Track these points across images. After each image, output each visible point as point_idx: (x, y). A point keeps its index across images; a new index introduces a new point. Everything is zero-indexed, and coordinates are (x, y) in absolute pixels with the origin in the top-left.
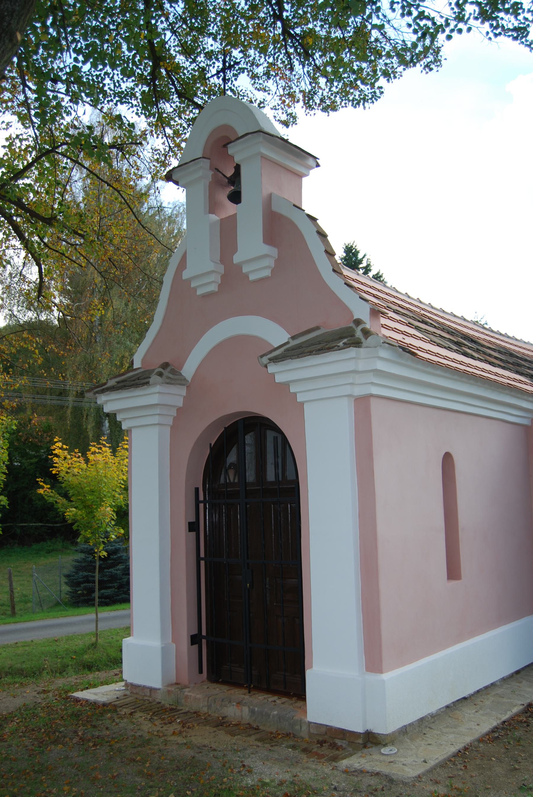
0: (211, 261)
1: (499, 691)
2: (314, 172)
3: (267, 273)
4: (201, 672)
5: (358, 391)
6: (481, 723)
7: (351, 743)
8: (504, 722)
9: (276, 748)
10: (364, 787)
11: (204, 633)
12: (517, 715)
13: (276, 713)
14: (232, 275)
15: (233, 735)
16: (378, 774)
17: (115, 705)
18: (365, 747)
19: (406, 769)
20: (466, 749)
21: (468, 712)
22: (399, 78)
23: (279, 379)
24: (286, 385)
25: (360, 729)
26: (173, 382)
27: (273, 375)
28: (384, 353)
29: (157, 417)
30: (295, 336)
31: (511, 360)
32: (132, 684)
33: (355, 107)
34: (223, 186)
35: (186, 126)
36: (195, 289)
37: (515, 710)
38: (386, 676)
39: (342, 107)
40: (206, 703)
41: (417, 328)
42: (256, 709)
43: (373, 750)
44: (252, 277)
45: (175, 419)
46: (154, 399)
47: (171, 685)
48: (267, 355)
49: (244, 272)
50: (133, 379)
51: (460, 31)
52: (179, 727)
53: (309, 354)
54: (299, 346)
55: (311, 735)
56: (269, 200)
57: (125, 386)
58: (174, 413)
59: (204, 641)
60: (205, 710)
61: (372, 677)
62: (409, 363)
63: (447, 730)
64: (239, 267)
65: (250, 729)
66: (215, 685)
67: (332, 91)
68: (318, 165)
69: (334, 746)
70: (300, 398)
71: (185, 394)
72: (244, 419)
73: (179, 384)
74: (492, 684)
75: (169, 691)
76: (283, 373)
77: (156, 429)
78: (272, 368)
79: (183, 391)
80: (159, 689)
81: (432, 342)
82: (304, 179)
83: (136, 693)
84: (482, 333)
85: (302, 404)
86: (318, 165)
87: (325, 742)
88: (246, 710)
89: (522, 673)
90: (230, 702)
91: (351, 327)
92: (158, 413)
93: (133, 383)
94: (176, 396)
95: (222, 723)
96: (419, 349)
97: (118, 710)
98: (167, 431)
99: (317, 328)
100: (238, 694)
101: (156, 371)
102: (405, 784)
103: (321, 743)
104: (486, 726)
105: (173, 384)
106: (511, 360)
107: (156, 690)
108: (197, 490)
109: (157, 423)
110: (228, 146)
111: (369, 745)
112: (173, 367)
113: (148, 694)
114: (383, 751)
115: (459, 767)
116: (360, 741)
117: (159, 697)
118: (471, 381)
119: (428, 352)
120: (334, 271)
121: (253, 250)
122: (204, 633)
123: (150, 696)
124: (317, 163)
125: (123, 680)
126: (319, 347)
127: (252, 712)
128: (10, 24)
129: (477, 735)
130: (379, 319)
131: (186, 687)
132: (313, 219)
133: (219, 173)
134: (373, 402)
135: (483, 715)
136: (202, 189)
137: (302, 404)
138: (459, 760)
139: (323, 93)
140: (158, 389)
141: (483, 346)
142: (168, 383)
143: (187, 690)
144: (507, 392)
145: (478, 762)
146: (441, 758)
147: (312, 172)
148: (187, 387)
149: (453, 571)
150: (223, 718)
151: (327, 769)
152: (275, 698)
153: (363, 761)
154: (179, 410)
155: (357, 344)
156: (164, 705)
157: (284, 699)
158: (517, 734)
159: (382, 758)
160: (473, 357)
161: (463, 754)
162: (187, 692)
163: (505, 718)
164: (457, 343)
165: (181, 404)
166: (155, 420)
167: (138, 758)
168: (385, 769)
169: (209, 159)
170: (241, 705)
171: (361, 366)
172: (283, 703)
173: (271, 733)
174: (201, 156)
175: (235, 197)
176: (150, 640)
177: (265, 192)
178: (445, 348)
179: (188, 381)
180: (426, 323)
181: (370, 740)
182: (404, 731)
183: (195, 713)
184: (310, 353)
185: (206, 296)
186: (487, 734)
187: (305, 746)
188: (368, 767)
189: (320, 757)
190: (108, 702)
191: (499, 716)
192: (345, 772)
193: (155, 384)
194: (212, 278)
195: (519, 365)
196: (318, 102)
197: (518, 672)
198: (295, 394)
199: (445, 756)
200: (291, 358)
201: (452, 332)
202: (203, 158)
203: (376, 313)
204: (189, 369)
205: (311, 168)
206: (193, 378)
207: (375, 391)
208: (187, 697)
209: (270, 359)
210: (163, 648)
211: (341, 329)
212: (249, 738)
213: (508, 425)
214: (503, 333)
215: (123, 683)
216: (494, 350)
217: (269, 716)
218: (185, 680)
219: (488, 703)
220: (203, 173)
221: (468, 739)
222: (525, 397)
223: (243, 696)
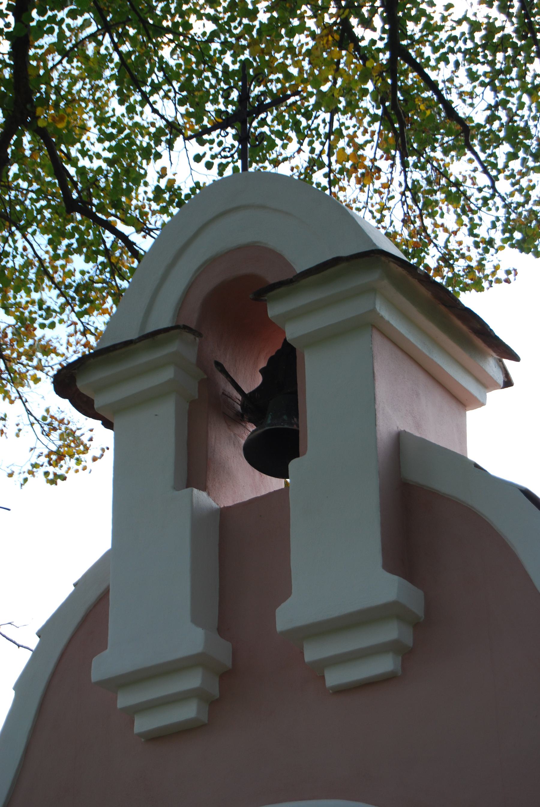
39: (498, 281)
68: (508, 383)
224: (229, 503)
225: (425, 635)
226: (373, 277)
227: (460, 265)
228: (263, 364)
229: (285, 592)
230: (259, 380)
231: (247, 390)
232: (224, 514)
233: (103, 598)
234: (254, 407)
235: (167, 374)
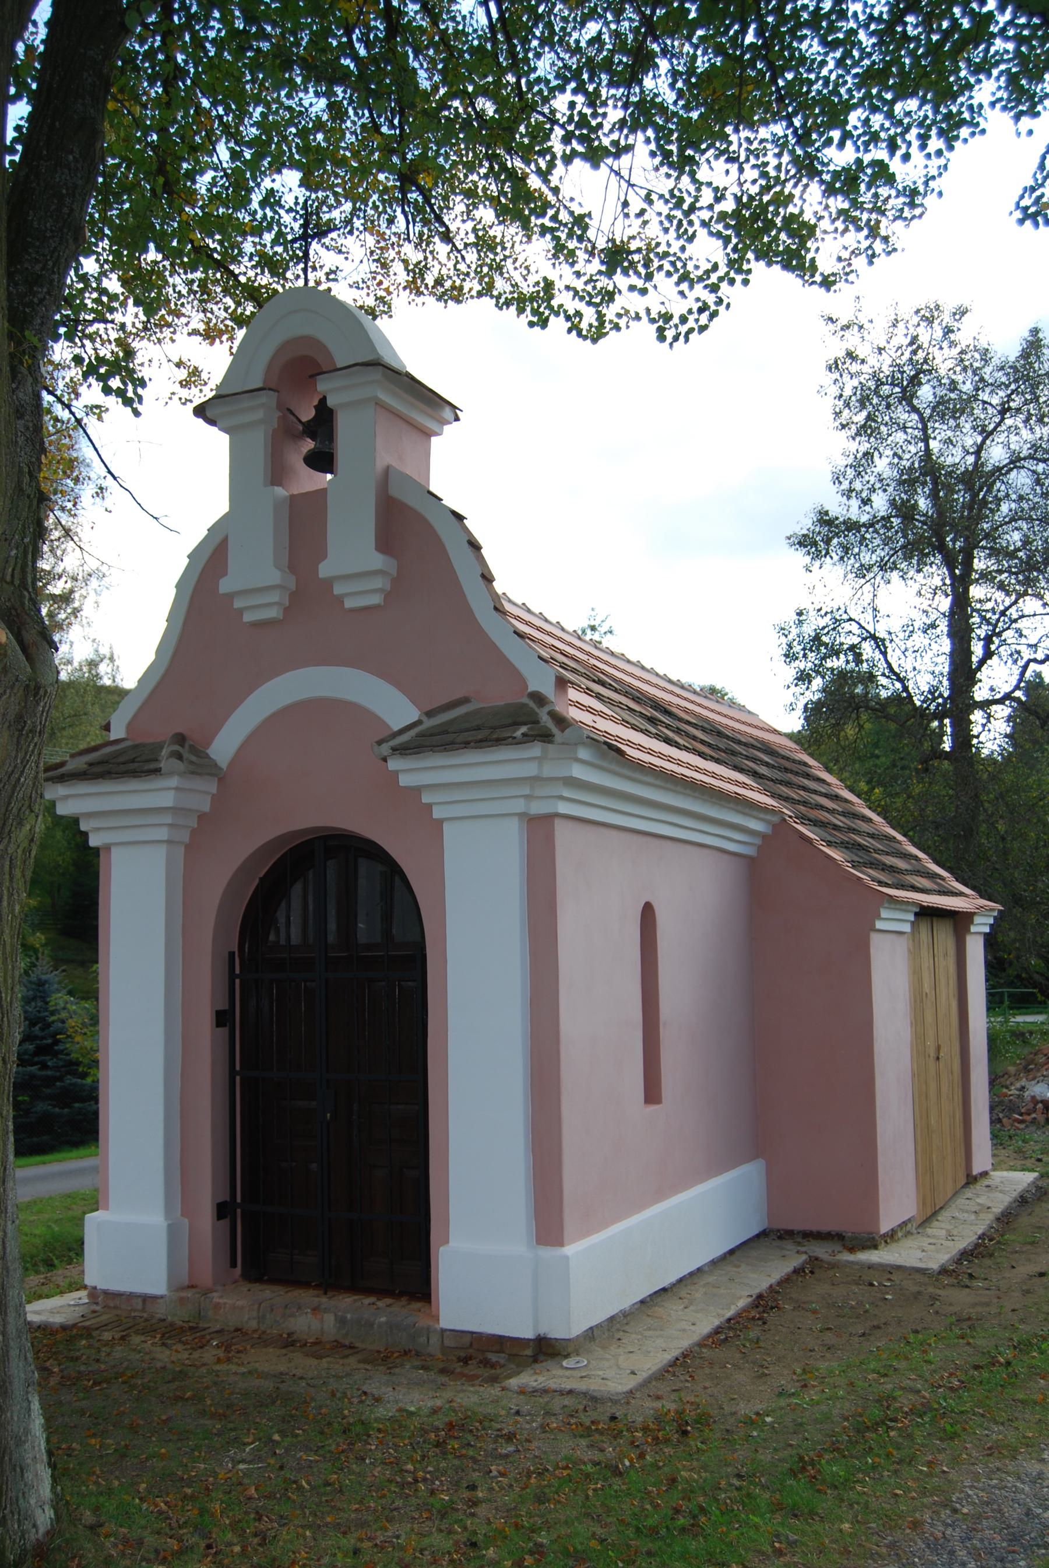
1: (711, 1279)
3: (376, 600)
4: (234, 1264)
5: (538, 808)
6: (694, 1323)
7: (512, 1357)
8: (729, 1320)
9: (397, 1370)
10: (557, 1409)
11: (239, 1200)
12: (745, 1310)
13: (383, 1319)
14: (307, 590)
15: (320, 1357)
16: (570, 1392)
17: (85, 1328)
18: (535, 1360)
19: (609, 1383)
20: (685, 1356)
21: (673, 1308)
23: (404, 780)
24: (417, 791)
25: (529, 1334)
27: (396, 774)
28: (583, 753)
31: (722, 744)
32: (106, 1293)
33: (501, 309)
34: (298, 437)
35: (184, 292)
36: (240, 612)
37: (741, 1303)
38: (570, 1250)
39: (472, 297)
40: (255, 1314)
41: (599, 697)
42: (349, 1316)
43: (549, 1364)
44: (349, 603)
45: (194, 832)
46: (167, 799)
47: (182, 1289)
51: (732, 282)
52: (221, 1353)
54: (443, 730)
55: (444, 1348)
57: (110, 773)
59: (239, 1211)
60: (254, 1324)
61: (547, 1253)
62: (613, 767)
63: (650, 1333)
65: (341, 1348)
66: (257, 1287)
68: (457, 419)
69: (486, 1363)
70: (437, 813)
74: (698, 1269)
75: (181, 1300)
76: (411, 772)
78: (393, 764)
79: (212, 787)
80: (162, 1297)
81: (625, 722)
82: (434, 440)
83: (115, 1308)
84: (664, 689)
85: (440, 822)
86: (457, 419)
87: (471, 1358)
88: (330, 1319)
89: (738, 1253)
90: (299, 1308)
91: (524, 706)
94: (201, 795)
95: (290, 1342)
96: (630, 743)
97: (95, 1333)
98: (181, 851)
99: (466, 700)
100: (307, 1297)
102: (615, 1402)
103: (465, 1361)
104: (706, 1325)
106: (722, 744)
107: (155, 1298)
108: (232, 955)
111: (541, 1357)
113: (140, 1306)
114: (565, 1363)
115: (682, 1378)
116: (529, 1352)
117: (160, 1311)
118: (688, 791)
119: (640, 747)
120: (496, 609)
121: (352, 554)
122: (239, 1200)
123: (143, 1310)
125: (85, 1287)
126: (481, 735)
127: (342, 1321)
128: (72, 210)
129: (696, 1338)
130: (566, 692)
131: (212, 1291)
132: (460, 518)
134: (559, 825)
135: (697, 1311)
137: (440, 822)
138: (679, 1371)
140: (174, 782)
141: (680, 720)
142: (193, 773)
143: (215, 1294)
144: (731, 805)
145: (707, 1371)
146: (654, 1369)
147: (447, 428)
149: (652, 1094)
150: (289, 1335)
151: (495, 1391)
152: (372, 1299)
153: (541, 1379)
154: (202, 817)
155: (546, 737)
156: (172, 1324)
157: (389, 1301)
158: (752, 1334)
159: (568, 1373)
160: (677, 746)
161: (681, 1363)
162: (216, 1297)
163: (729, 1314)
164: (652, 720)
165: (206, 808)
167: (189, 1394)
168: (581, 1386)
170: (316, 1314)
171: (549, 770)
172: (389, 1306)
173: (378, 1352)
174: (260, 385)
176: (136, 1214)
177: (380, 464)
178: (641, 731)
179: (221, 769)
180: (603, 683)
181: (545, 1349)
182: (591, 1334)
183: (237, 1330)
184: (466, 745)
186: (709, 1336)
187: (441, 1365)
188: (553, 1384)
189: (471, 1379)
190: (70, 1323)
191: (721, 1312)
192: (522, 1392)
193: (171, 774)
195: (734, 753)
196: (431, 283)
197: (732, 1252)
198: (429, 807)
199: (660, 1366)
201: (639, 697)
203: (562, 683)
204: (224, 747)
206: (233, 763)
207: (563, 808)
208: (217, 1307)
209: (394, 749)
210: (169, 1226)
212: (346, 1361)
213: (726, 857)
214: (674, 679)
215: (83, 1293)
216: (694, 726)
217: (372, 1325)
218: (206, 1277)
219: (698, 1295)
220: (262, 412)
221: (685, 1343)
222: (755, 813)
223: (317, 1299)
224: (295, 493)
225: (398, 590)
226: (377, 374)
227: (448, 284)
228: (316, 403)
229: (323, 555)
230: (312, 413)
231: (304, 419)
232: (292, 497)
233: (225, 540)
234: (311, 429)
235: (260, 415)
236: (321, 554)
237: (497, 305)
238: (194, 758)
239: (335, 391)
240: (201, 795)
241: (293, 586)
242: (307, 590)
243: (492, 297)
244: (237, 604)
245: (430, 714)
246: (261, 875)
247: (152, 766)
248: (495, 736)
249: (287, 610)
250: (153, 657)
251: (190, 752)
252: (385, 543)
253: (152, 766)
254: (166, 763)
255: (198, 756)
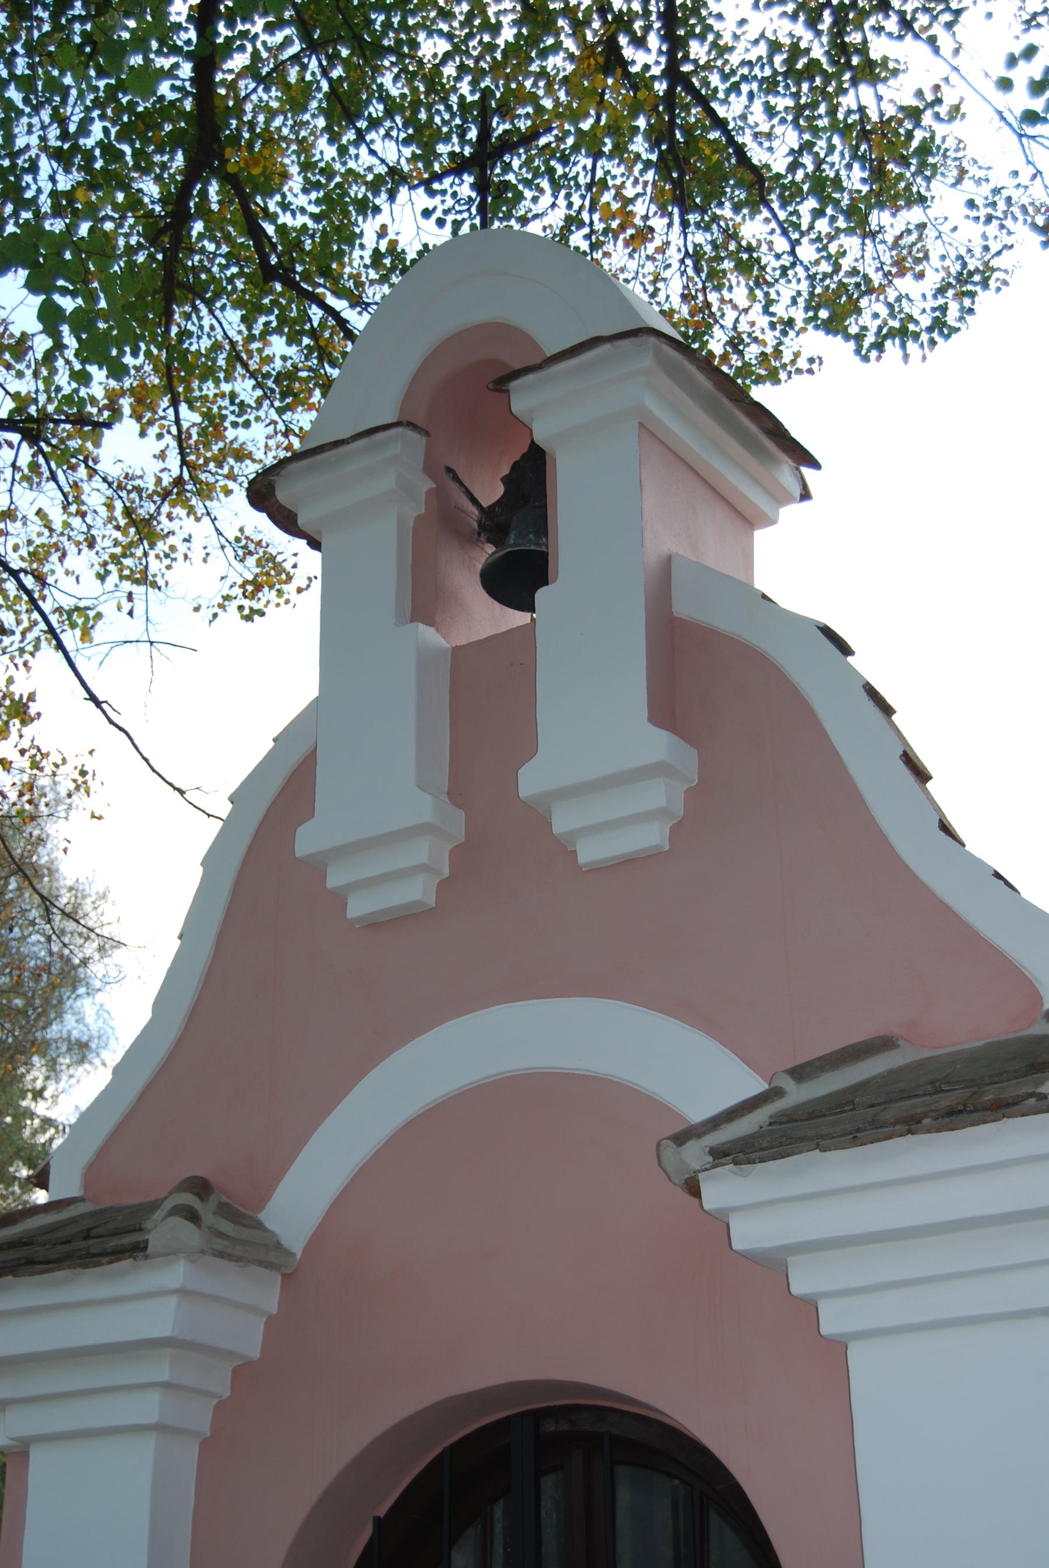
0: (418, 786)
2: (790, 513)
14: (496, 837)
22: (998, 289)
23: (747, 1234)
24: (772, 1265)
26: (238, 1251)
29: (155, 1397)
30: (802, 1066)
33: (866, 359)
36: (340, 898)
39: (799, 371)
44: (589, 852)
45: (222, 1410)
46: (158, 1319)
48: (699, 1136)
49: (557, 829)
50: (60, 1234)
53: (902, 1128)
54: (842, 1102)
56: (662, 580)
58: (220, 1383)
64: (536, 818)
67: (773, 315)
68: (806, 495)
71: (274, 1310)
72: (537, 1416)
73: (261, 1263)
76: (761, 1208)
77: (146, 1448)
78: (720, 1190)
79: (266, 1294)
82: (761, 537)
92: (165, 1377)
93: (62, 1249)
94: (241, 1311)
98: (189, 1454)
99: (884, 1044)
101: (168, 1205)
105: (238, 1259)
109: (153, 1419)
110: (514, 384)
112: (224, 1199)
124: (805, 486)
126: (945, 1102)
133: (454, 487)
136: (383, 543)
139: (737, 321)
140: (176, 1274)
142: (221, 1255)
148: (285, 1276)
154: (244, 1373)
165: (254, 1350)
166: (147, 1408)
169: (427, 434)
175: (518, 577)
179: (290, 1254)
184: (911, 1125)
185: (377, 925)
193: (171, 1253)
194: (419, 852)
200: (818, 1147)
202: (411, 425)
204: (298, 1204)
205: (784, 499)
206: (318, 1240)
211: (991, 1046)
220: (388, 488)
224: (463, 641)
225: (701, 816)
230: (500, 490)
233: (310, 760)
236: (526, 746)
237: (858, 351)
238: (226, 1226)
239: (544, 409)
240: (241, 1311)
241: (460, 835)
242: (496, 837)
243: (847, 337)
244: (335, 879)
245: (800, 1073)
246: (382, 1511)
247: (128, 1240)
248: (988, 1097)
249: (444, 886)
250: (146, 1015)
251: (223, 1214)
252: (667, 709)
253: (128, 1240)
254: (162, 1231)
255: (236, 1222)
